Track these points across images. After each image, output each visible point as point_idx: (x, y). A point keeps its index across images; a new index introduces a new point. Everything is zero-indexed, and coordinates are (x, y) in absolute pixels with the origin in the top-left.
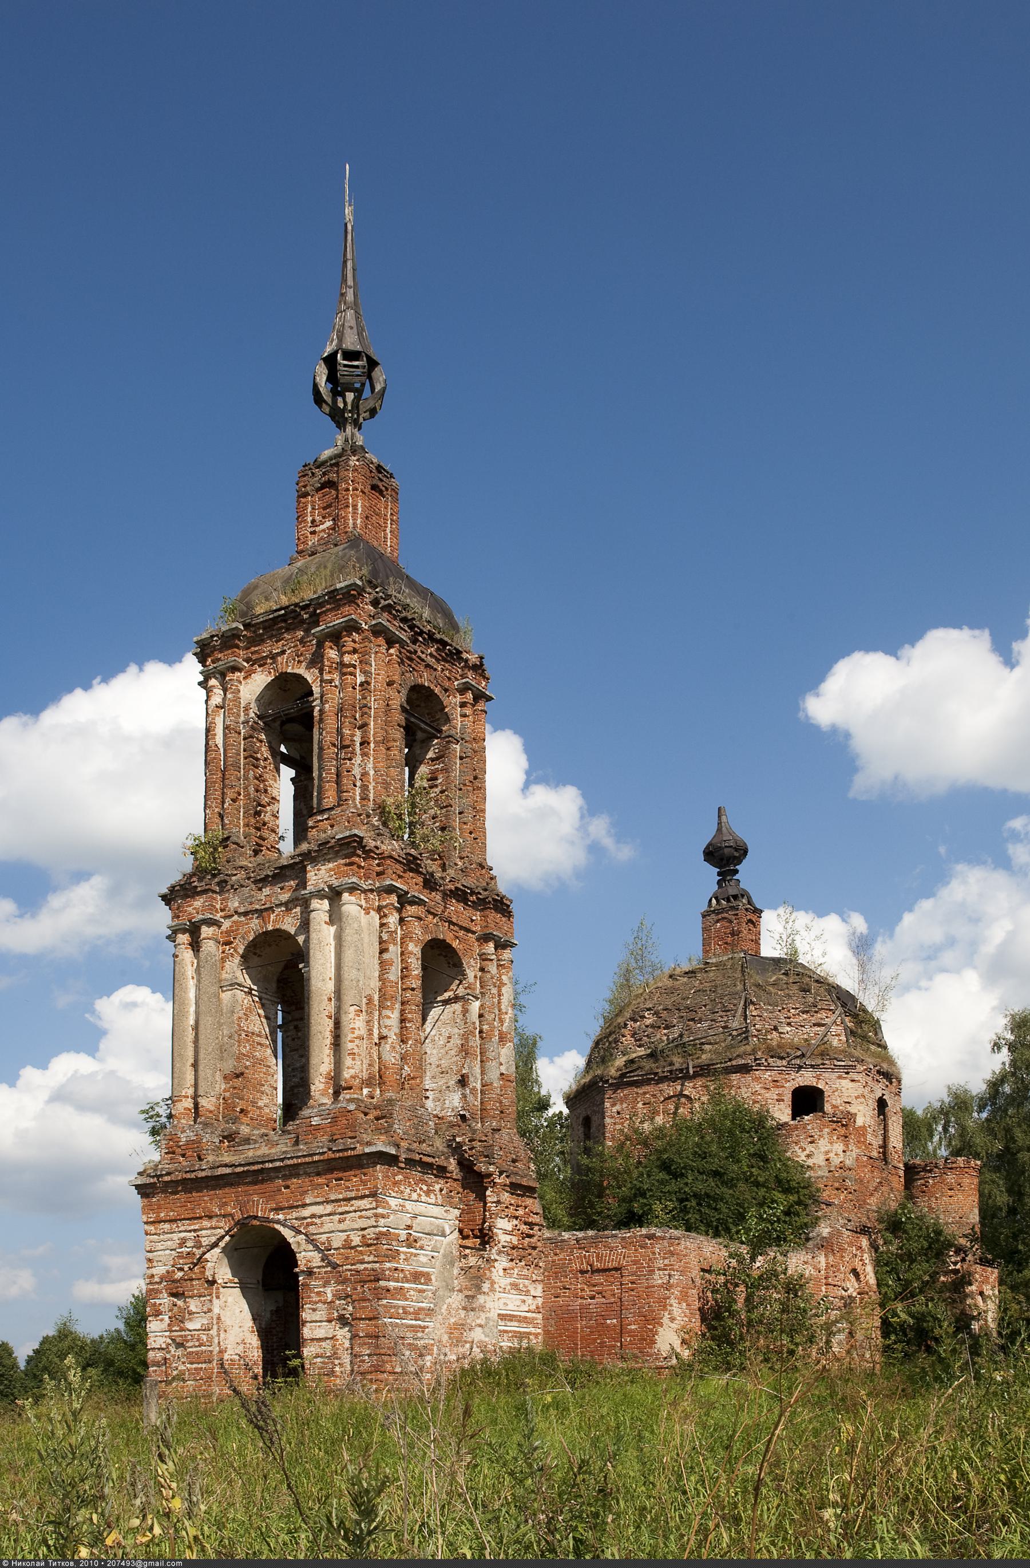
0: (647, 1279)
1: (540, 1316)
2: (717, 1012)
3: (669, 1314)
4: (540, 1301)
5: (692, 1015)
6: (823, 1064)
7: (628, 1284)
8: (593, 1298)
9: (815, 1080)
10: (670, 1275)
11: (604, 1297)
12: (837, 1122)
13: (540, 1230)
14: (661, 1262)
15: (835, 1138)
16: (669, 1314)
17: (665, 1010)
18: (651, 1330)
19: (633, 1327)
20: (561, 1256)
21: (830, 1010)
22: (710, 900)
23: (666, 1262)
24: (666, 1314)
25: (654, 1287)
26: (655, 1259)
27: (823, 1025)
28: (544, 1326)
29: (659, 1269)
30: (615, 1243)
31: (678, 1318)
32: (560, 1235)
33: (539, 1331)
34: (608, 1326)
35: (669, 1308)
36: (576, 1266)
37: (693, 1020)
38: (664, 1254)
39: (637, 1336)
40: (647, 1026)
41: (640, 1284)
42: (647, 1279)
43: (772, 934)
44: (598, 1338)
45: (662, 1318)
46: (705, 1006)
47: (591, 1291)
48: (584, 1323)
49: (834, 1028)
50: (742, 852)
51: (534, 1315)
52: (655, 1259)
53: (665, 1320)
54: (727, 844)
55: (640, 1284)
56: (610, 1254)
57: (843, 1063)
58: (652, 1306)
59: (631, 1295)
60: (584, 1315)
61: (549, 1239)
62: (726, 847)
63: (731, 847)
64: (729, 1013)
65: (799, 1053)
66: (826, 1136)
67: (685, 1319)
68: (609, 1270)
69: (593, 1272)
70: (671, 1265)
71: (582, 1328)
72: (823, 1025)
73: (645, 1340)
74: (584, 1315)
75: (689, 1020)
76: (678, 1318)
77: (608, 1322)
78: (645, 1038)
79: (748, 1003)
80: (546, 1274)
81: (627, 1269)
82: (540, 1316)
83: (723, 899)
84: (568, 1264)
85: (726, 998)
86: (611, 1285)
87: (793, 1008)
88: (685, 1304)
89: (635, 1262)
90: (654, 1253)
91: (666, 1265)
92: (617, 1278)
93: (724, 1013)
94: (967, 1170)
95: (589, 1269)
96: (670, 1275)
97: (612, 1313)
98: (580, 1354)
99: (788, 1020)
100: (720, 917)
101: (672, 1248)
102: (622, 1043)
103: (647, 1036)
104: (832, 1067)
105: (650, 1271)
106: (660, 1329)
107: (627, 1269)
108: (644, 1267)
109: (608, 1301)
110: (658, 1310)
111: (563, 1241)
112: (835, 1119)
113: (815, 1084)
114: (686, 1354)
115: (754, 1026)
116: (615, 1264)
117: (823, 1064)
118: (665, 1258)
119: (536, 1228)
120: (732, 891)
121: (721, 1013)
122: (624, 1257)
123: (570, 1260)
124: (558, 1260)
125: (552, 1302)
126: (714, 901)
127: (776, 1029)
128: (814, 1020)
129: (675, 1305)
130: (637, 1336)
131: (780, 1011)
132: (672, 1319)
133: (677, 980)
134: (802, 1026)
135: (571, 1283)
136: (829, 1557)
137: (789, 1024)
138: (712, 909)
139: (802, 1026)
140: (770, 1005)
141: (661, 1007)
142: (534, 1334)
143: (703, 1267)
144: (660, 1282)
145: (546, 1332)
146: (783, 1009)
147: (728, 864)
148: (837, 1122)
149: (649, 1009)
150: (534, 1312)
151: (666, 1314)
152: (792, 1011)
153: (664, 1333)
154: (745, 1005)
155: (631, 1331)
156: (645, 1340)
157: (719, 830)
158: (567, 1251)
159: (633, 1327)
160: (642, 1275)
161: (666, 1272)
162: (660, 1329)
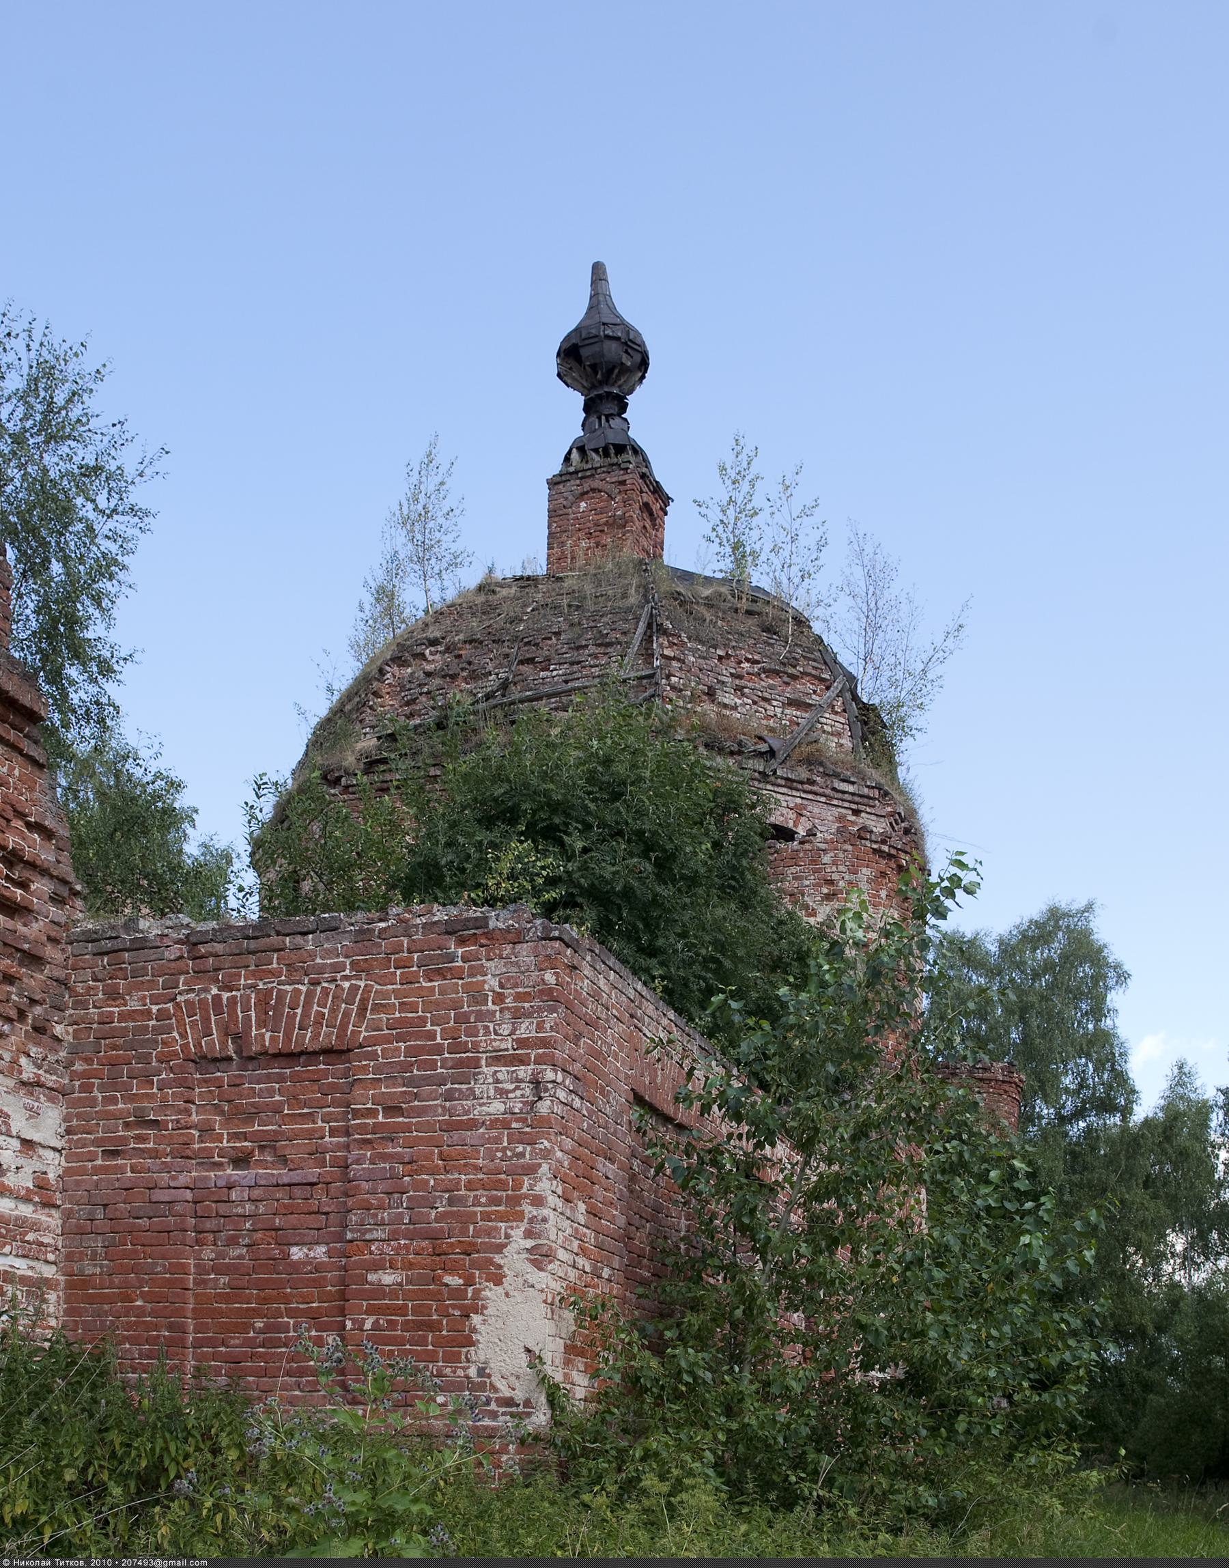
0: (449, 1096)
1: (53, 1220)
2: (587, 646)
3: (529, 1234)
4: (53, 1165)
5: (529, 652)
6: (813, 783)
7: (372, 1113)
8: (241, 1161)
9: (792, 815)
10: (536, 1083)
11: (283, 1160)
12: (890, 856)
13: (57, 900)
14: (505, 1029)
15: (883, 894)
16: (529, 1234)
17: (470, 642)
18: (458, 1293)
19: (388, 1278)
20: (133, 1005)
21: (822, 680)
22: (570, 452)
23: (526, 1029)
24: (517, 1233)
25: (472, 1125)
26: (480, 1016)
27: (807, 707)
28: (69, 1257)
29: (498, 1059)
30: (328, 953)
31: (562, 1254)
32: (131, 924)
33: (49, 1272)
34: (296, 1266)
35: (528, 1209)
36: (179, 1040)
37: (531, 661)
38: (519, 997)
39: (402, 1311)
40: (429, 674)
41: (422, 1111)
42: (449, 1096)
43: (703, 510)
44: (257, 1313)
45: (500, 1248)
46: (557, 634)
47: (234, 1137)
48: (208, 1253)
49: (828, 719)
50: (638, 358)
51: (26, 1210)
52: (480, 1016)
53: (514, 1259)
54: (609, 332)
55: (422, 1111)
56: (310, 995)
57: (851, 788)
58: (461, 1200)
59: (385, 1157)
60: (209, 1225)
61: (91, 938)
62: (608, 337)
63: (618, 339)
64: (609, 650)
65: (763, 747)
66: (864, 886)
67: (581, 1261)
68: (311, 1055)
69: (249, 1059)
70: (544, 1043)
71: (201, 1269)
72: (807, 707)
73: (433, 1327)
74: (209, 1225)
75: (522, 662)
76: (562, 1254)
77: (297, 1253)
78: (423, 699)
79: (654, 629)
80: (79, 1066)
81: (373, 1056)
82: (53, 1220)
83: (596, 451)
84: (157, 1031)
85: (605, 619)
86: (310, 1117)
87: (748, 660)
88: (582, 1207)
89: (403, 1029)
90: (478, 996)
91: (522, 1043)
92: (334, 1088)
93: (601, 650)
94: (1006, 1086)
95: (231, 1049)
96: (536, 1083)
97: (313, 1221)
98: (191, 1364)
99: (737, 682)
100: (586, 488)
101: (550, 977)
102: (371, 708)
103: (429, 693)
104: (828, 791)
105: (460, 1064)
106: (492, 1293)
107: (373, 1056)
108: (438, 1050)
109: (296, 1177)
110: (487, 1217)
111: (140, 945)
112: (886, 848)
113: (791, 825)
114: (580, 1386)
115: (668, 677)
116: (327, 1036)
117: (813, 783)
118: (517, 1015)
119: (41, 886)
120: (613, 438)
121: (592, 649)
122: (362, 1010)
123: (163, 1015)
124: (123, 1017)
125: (97, 1170)
126: (575, 455)
127: (711, 694)
128: (789, 693)
129: (552, 1200)
130: (402, 1311)
131: (720, 658)
132: (540, 1257)
133: (494, 592)
134: (764, 699)
135: (164, 1108)
136: (505, 1553)
137: (739, 690)
138: (572, 469)
139: (764, 699)
140: (701, 642)
141: (461, 637)
142: (24, 1280)
143: (641, 1091)
144: (497, 1107)
145: (77, 1285)
146: (728, 656)
147: (606, 381)
148: (890, 856)
149: (433, 642)
150: (27, 1200)
151: (517, 1233)
152: (746, 665)
153: (505, 1305)
154: (648, 639)
155: (380, 1291)
156: (433, 1327)
157: (593, 307)
158: (152, 984)
159: (388, 1278)
160: (428, 1081)
161: (524, 1072)
162: (492, 1293)
